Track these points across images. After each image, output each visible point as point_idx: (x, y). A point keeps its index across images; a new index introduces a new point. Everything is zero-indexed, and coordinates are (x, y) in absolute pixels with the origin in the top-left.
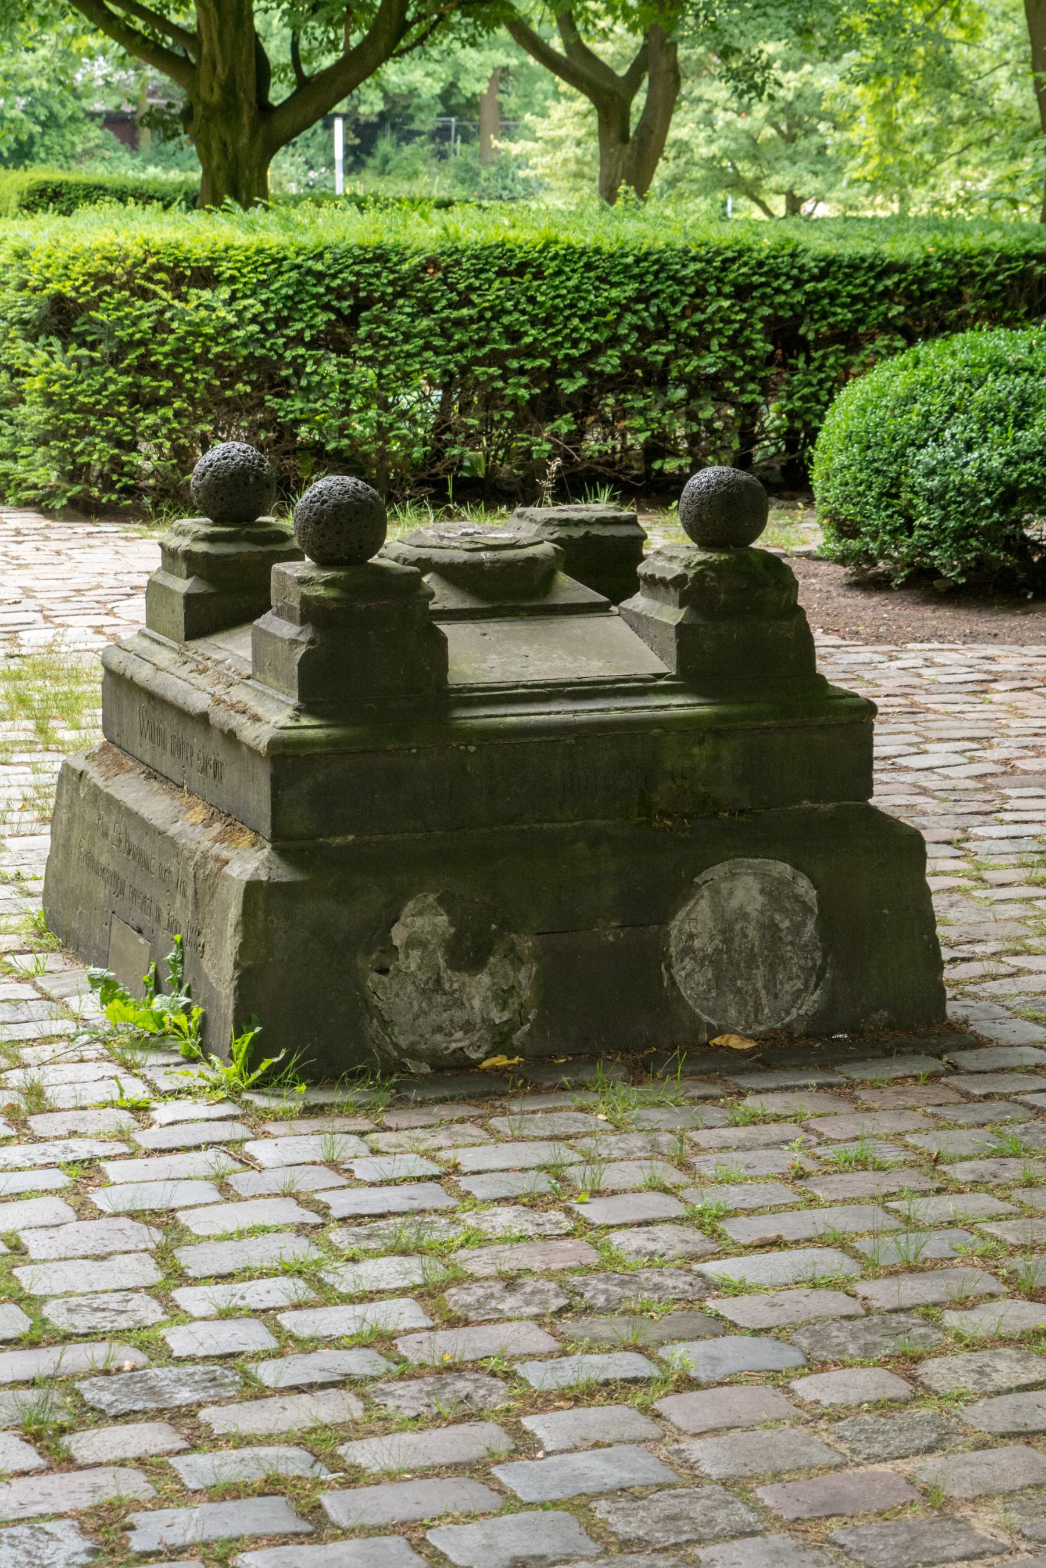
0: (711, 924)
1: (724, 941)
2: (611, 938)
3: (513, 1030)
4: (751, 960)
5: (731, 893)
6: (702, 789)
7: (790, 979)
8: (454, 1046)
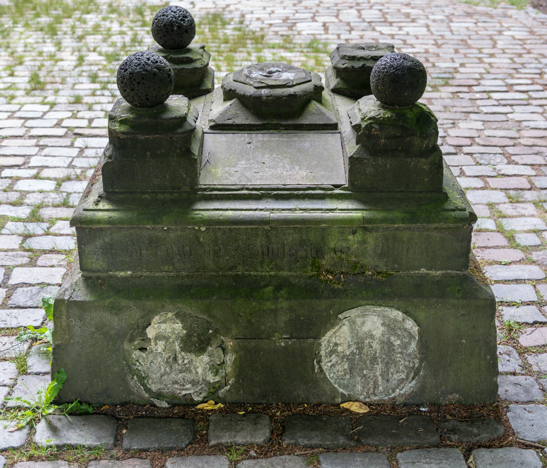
0: (350, 339)
1: (358, 348)
2: (283, 344)
3: (220, 387)
4: (374, 360)
5: (363, 323)
6: (354, 259)
7: (397, 372)
8: (184, 392)
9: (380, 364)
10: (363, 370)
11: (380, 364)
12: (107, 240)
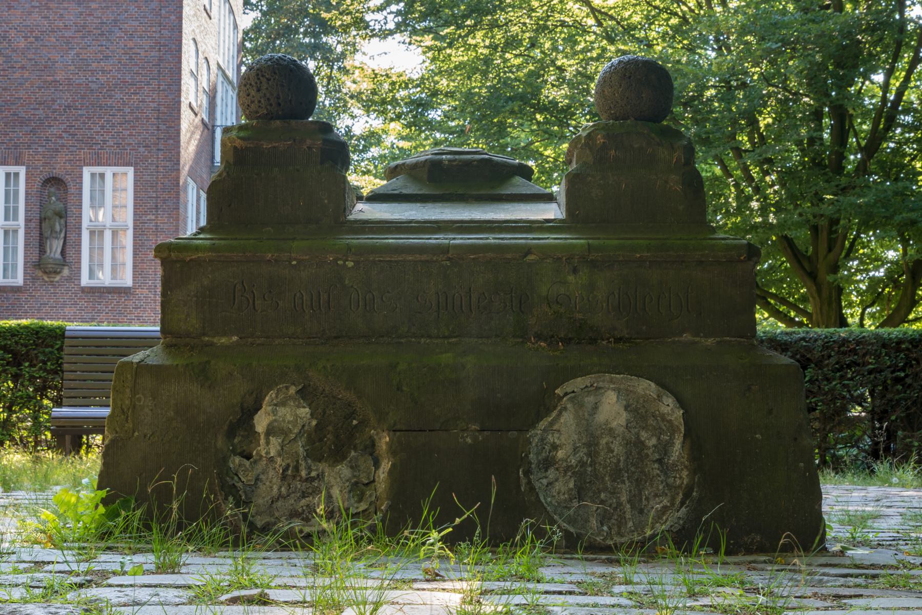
1: (589, 455)
2: (469, 440)
6: (579, 316)
7: (656, 495)
9: (627, 482)
10: (600, 492)
11: (627, 482)
12: (206, 282)
